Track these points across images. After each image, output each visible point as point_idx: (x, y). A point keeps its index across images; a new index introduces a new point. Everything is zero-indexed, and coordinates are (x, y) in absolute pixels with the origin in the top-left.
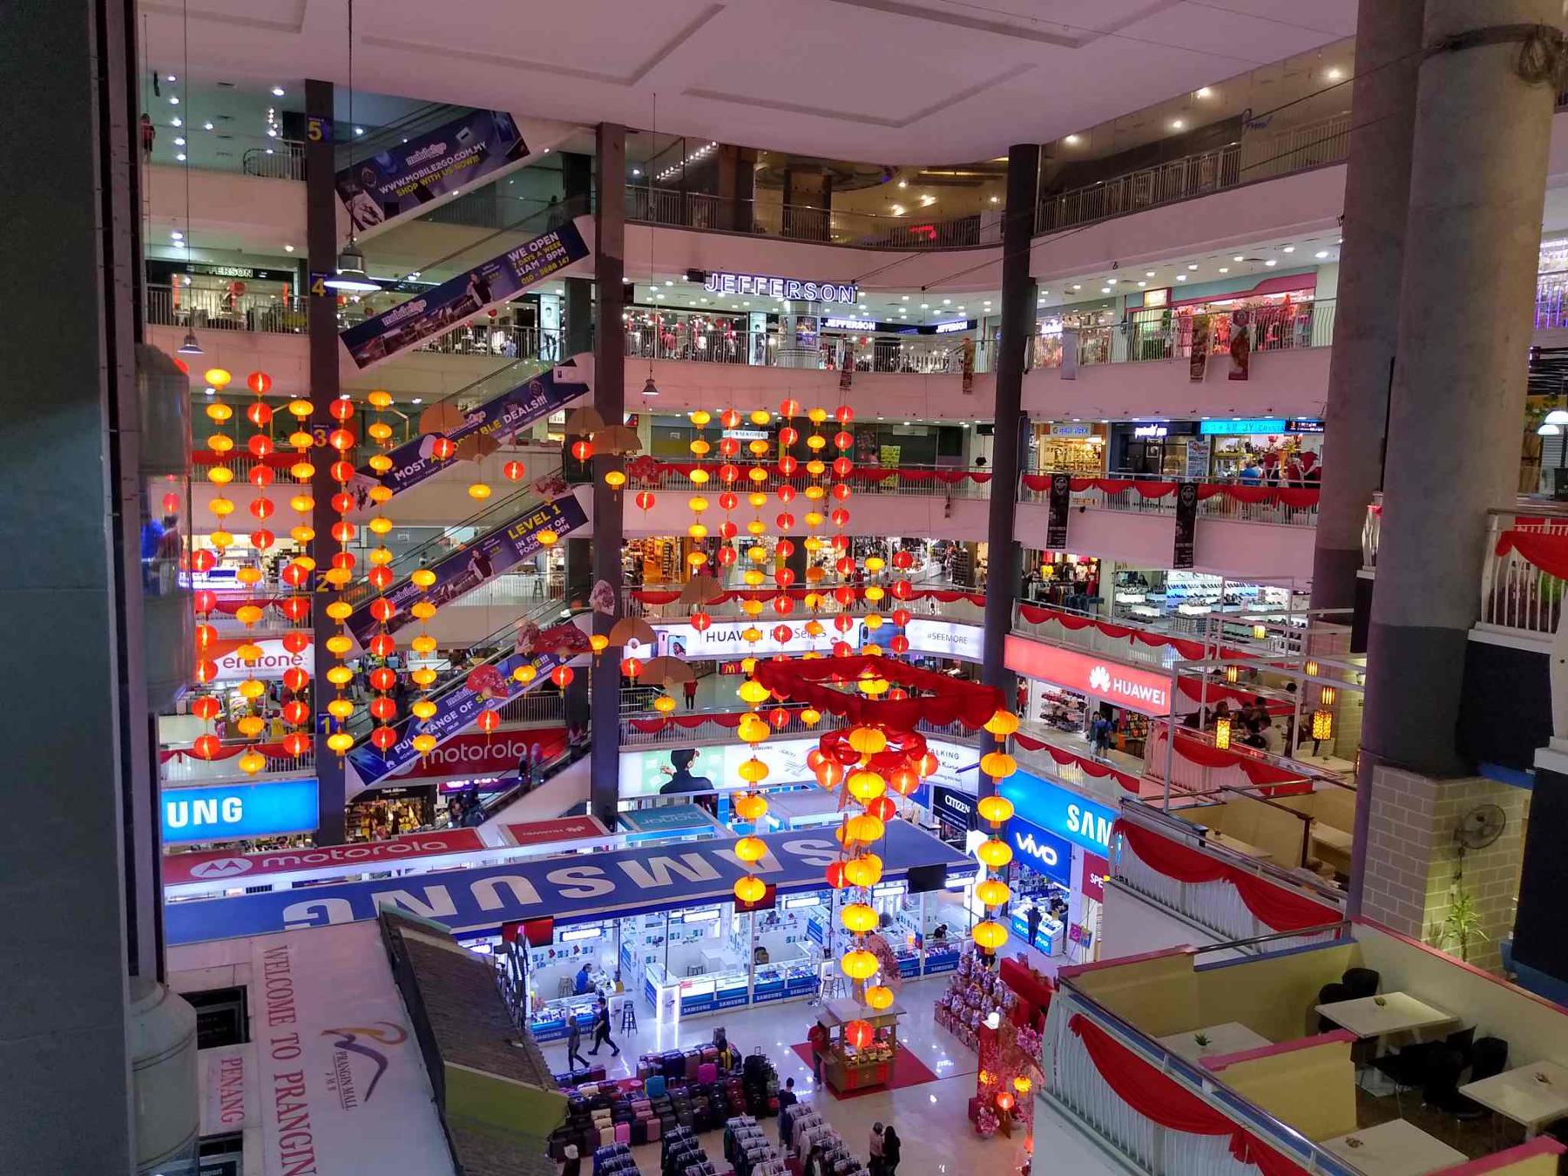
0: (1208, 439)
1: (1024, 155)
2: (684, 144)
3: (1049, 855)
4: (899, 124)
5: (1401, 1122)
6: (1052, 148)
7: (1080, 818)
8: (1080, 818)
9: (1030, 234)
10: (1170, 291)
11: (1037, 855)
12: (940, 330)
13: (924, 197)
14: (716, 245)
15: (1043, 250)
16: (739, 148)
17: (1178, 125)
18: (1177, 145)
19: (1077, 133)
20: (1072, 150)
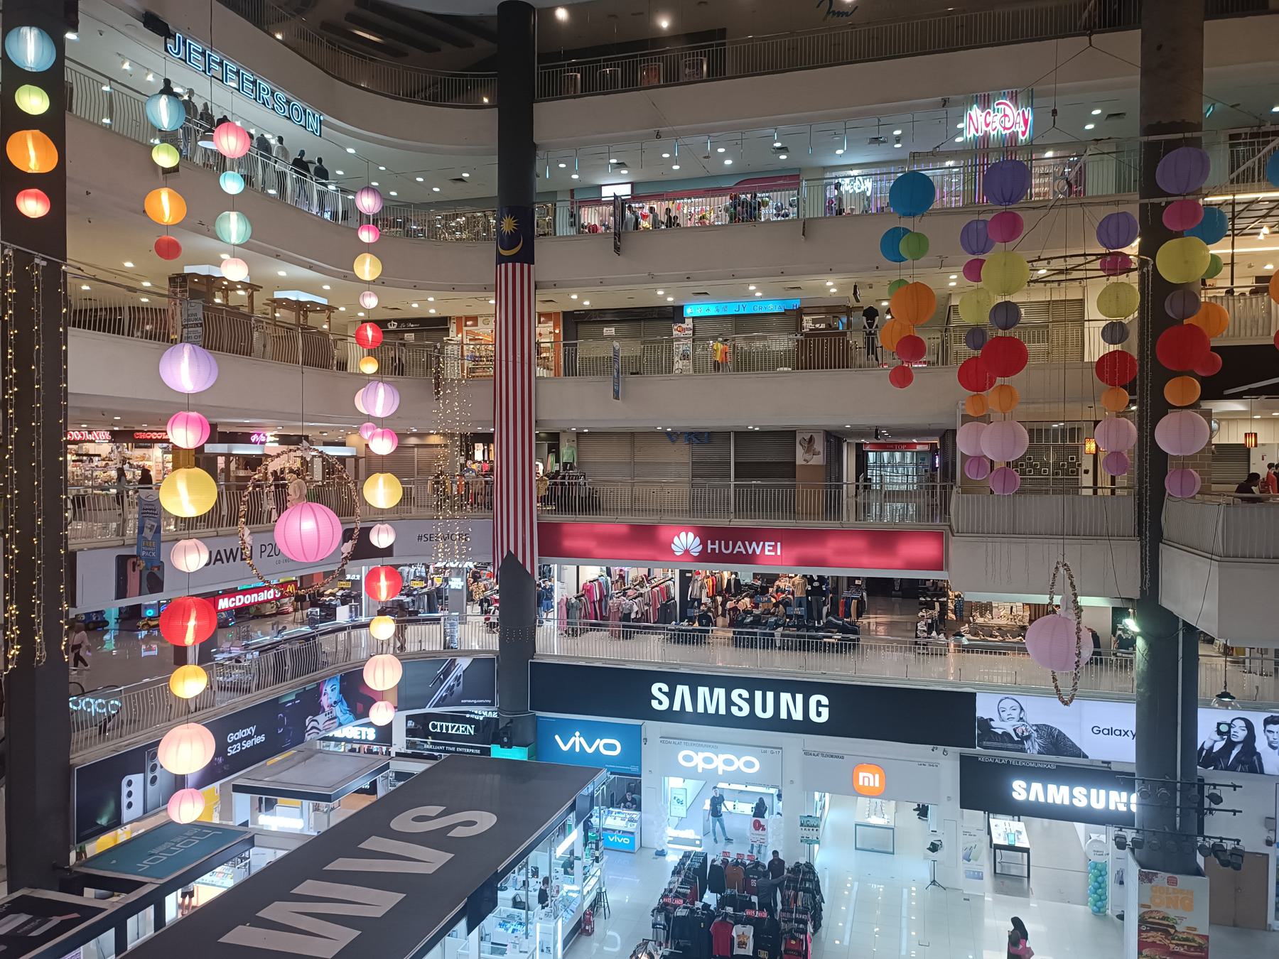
0: (689, 323)
3: (610, 747)
8: (671, 695)
15: (552, 119)
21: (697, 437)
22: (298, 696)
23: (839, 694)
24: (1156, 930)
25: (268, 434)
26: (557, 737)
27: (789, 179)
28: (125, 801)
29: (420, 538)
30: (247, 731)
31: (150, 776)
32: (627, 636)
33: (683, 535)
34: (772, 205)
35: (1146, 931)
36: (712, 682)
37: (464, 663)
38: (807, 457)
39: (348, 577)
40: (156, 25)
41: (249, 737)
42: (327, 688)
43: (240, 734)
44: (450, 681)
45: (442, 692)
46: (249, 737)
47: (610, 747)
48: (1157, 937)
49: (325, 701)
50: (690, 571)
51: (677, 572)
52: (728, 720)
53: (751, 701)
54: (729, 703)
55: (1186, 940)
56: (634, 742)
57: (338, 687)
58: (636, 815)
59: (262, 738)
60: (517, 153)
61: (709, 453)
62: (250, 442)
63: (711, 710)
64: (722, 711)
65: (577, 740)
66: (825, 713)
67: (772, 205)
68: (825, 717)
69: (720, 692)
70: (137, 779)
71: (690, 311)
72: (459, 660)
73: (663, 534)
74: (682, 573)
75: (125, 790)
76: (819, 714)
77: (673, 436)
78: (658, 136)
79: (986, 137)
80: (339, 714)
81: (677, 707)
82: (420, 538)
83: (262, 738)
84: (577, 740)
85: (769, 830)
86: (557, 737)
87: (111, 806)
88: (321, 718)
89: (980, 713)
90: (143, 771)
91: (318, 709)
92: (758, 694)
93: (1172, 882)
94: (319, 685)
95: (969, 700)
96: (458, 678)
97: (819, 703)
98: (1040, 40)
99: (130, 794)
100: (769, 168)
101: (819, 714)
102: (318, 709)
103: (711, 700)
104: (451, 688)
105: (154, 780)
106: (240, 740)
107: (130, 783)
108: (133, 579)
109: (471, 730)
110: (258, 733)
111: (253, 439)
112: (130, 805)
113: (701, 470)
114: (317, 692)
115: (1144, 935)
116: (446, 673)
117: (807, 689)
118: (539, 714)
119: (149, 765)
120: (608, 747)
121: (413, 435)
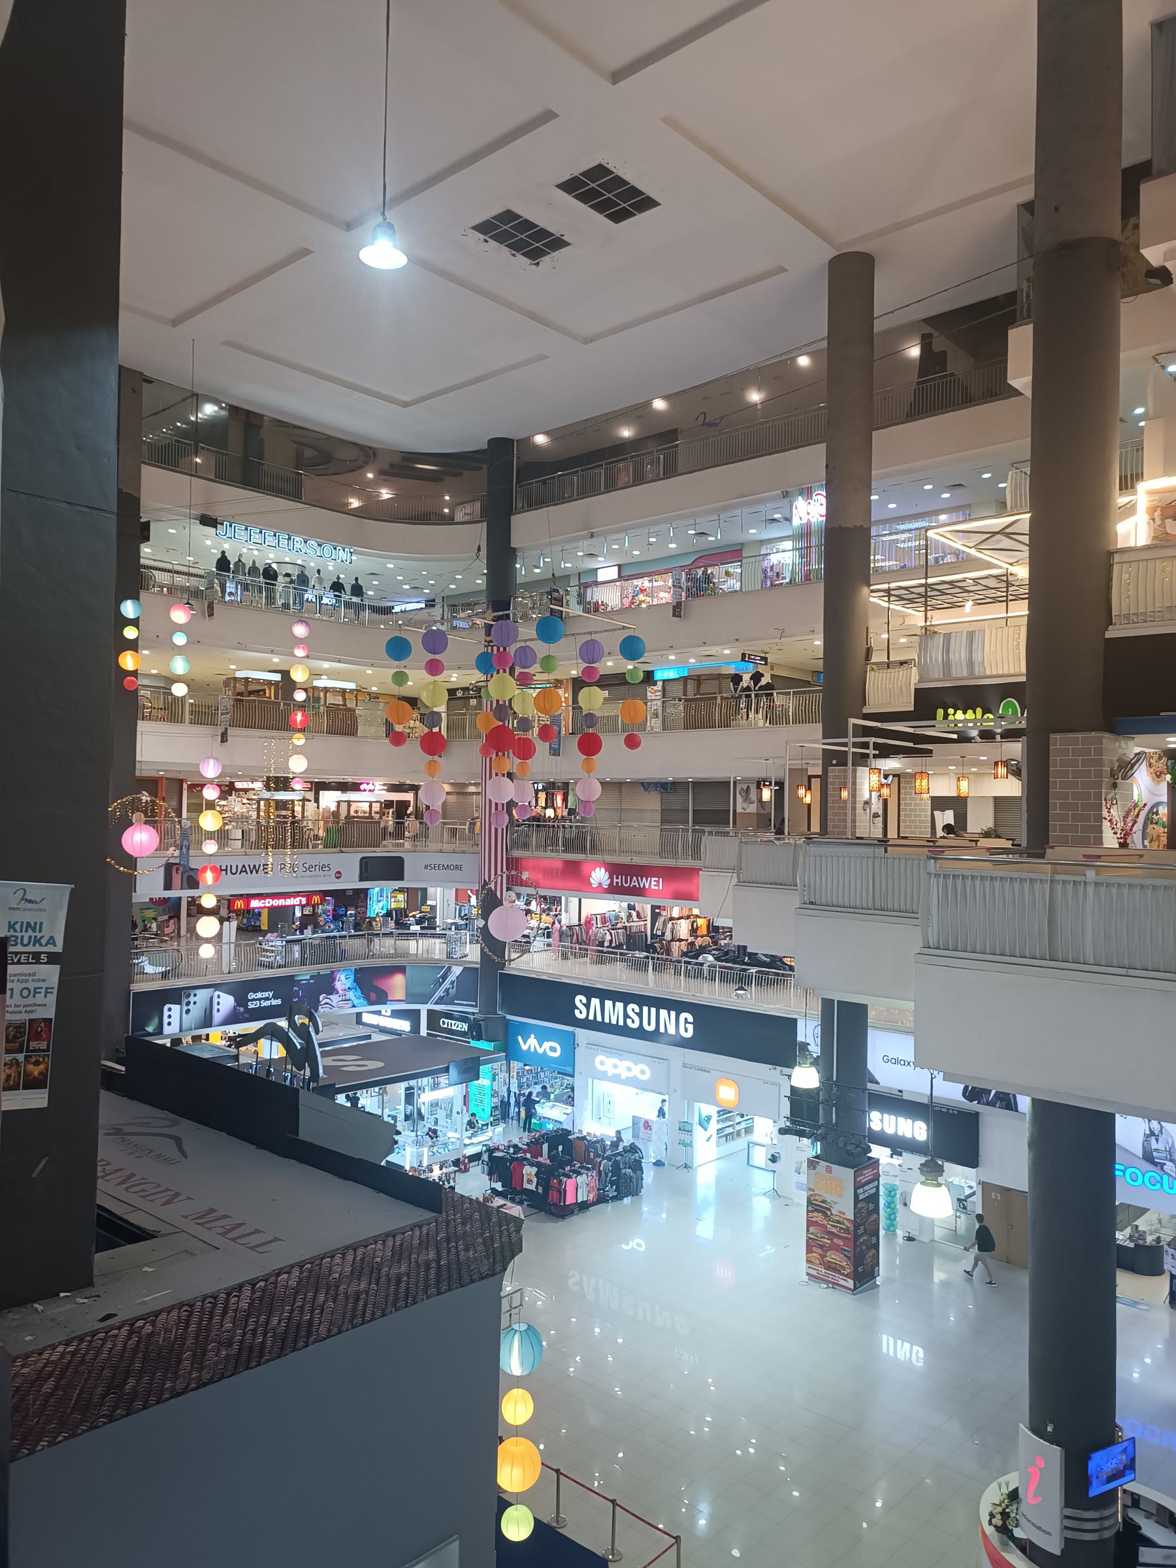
0: (660, 684)
1: (501, 447)
2: (196, 399)
3: (553, 1049)
4: (406, 404)
5: (499, 1482)
6: (527, 442)
7: (587, 1006)
8: (587, 1006)
9: (510, 511)
10: (620, 566)
11: (540, 1051)
12: (397, 609)
13: (351, 500)
14: (229, 496)
15: (525, 527)
16: (248, 412)
17: (626, 433)
18: (622, 448)
19: (546, 433)
20: (537, 447)
21: (665, 787)
22: (312, 977)
23: (704, 1015)
24: (819, 1211)
25: (377, 784)
26: (520, 1038)
27: (733, 553)
28: (166, 1020)
29: (426, 867)
30: (266, 994)
31: (185, 1008)
32: (601, 962)
33: (598, 869)
34: (729, 578)
35: (812, 1212)
36: (616, 996)
37: (457, 970)
38: (745, 805)
39: (429, 902)
40: (208, 521)
41: (267, 999)
42: (341, 976)
43: (259, 995)
44: (447, 984)
45: (440, 992)
46: (267, 999)
47: (553, 1049)
48: (817, 1217)
49: (338, 985)
50: (659, 907)
51: (649, 907)
52: (622, 1030)
53: (640, 1015)
54: (626, 1016)
55: (838, 1222)
56: (570, 1046)
57: (352, 977)
58: (569, 1109)
59: (279, 1002)
60: (501, 555)
61: (675, 800)
62: (360, 790)
63: (614, 1022)
64: (621, 1023)
65: (532, 1042)
66: (690, 1027)
67: (729, 578)
68: (690, 1034)
69: (619, 1005)
70: (176, 1008)
71: (659, 675)
72: (454, 968)
73: (585, 868)
74: (653, 908)
75: (166, 1013)
76: (686, 1030)
77: (646, 786)
78: (592, 536)
79: (809, 524)
80: (353, 998)
81: (591, 1017)
82: (426, 867)
83: (279, 1002)
84: (532, 1042)
85: (654, 1130)
86: (520, 1038)
87: (156, 1021)
88: (335, 998)
89: (800, 1038)
90: (180, 1004)
91: (332, 990)
92: (645, 1009)
93: (829, 1170)
94: (333, 972)
95: (793, 1022)
96: (452, 983)
97: (686, 1021)
98: (770, 454)
99: (170, 1017)
100: (726, 546)
101: (686, 1030)
102: (332, 990)
103: (614, 1012)
104: (447, 990)
105: (188, 1011)
106: (260, 999)
107: (170, 1010)
108: (177, 879)
109: (465, 1027)
110: (275, 997)
111: (362, 787)
112: (169, 1024)
113: (668, 817)
114: (331, 978)
115: (811, 1215)
116: (444, 977)
117: (677, 1006)
118: (509, 1017)
119: (185, 1001)
120: (551, 1049)
121: (474, 784)
